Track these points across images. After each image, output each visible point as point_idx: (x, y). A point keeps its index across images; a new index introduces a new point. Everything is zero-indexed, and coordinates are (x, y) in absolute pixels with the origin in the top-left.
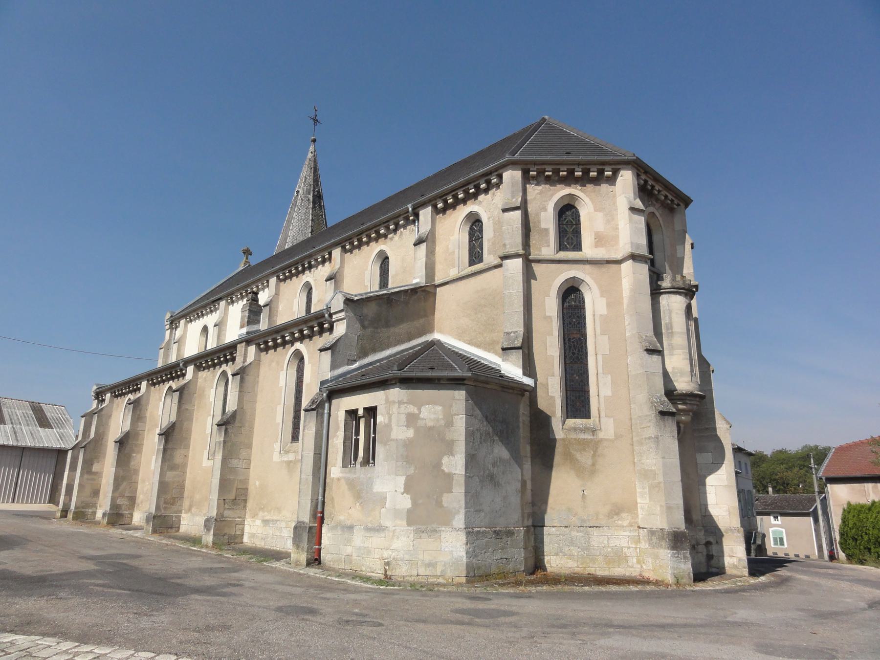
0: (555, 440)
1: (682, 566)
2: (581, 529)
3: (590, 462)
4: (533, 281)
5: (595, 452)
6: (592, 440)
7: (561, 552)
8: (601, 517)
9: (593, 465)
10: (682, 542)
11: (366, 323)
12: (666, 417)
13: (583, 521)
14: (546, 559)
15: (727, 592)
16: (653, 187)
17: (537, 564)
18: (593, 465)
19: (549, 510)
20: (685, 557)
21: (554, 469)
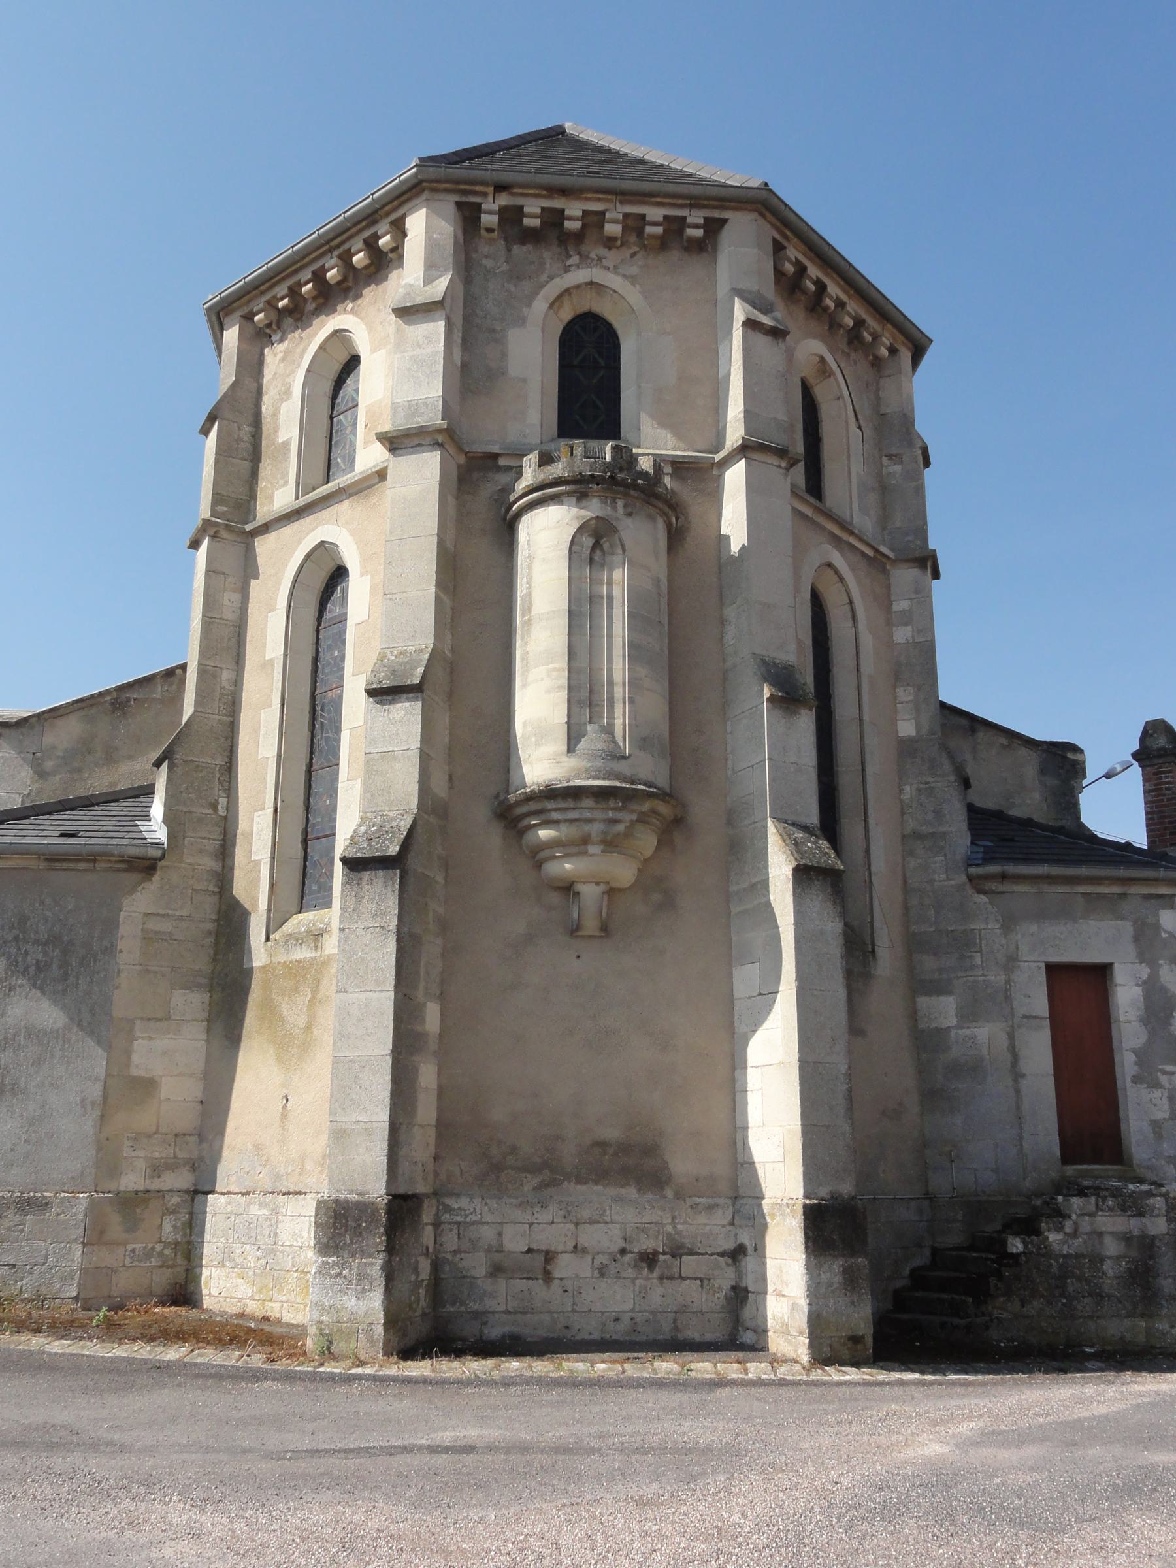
0: (248, 973)
1: (351, 1303)
2: (268, 1198)
3: (302, 1021)
4: (253, 582)
5: (315, 992)
6: (314, 959)
7: (231, 1259)
8: (309, 1166)
9: (308, 1028)
10: (358, 1233)
11: (49, 765)
12: (366, 875)
13: (278, 1177)
14: (205, 1273)
15: (558, 1383)
16: (821, 287)
17: (184, 1294)
18: (308, 1028)
19: (226, 1153)
20: (362, 1278)
21: (243, 1045)
